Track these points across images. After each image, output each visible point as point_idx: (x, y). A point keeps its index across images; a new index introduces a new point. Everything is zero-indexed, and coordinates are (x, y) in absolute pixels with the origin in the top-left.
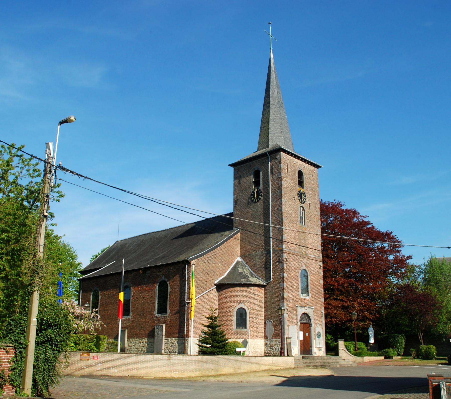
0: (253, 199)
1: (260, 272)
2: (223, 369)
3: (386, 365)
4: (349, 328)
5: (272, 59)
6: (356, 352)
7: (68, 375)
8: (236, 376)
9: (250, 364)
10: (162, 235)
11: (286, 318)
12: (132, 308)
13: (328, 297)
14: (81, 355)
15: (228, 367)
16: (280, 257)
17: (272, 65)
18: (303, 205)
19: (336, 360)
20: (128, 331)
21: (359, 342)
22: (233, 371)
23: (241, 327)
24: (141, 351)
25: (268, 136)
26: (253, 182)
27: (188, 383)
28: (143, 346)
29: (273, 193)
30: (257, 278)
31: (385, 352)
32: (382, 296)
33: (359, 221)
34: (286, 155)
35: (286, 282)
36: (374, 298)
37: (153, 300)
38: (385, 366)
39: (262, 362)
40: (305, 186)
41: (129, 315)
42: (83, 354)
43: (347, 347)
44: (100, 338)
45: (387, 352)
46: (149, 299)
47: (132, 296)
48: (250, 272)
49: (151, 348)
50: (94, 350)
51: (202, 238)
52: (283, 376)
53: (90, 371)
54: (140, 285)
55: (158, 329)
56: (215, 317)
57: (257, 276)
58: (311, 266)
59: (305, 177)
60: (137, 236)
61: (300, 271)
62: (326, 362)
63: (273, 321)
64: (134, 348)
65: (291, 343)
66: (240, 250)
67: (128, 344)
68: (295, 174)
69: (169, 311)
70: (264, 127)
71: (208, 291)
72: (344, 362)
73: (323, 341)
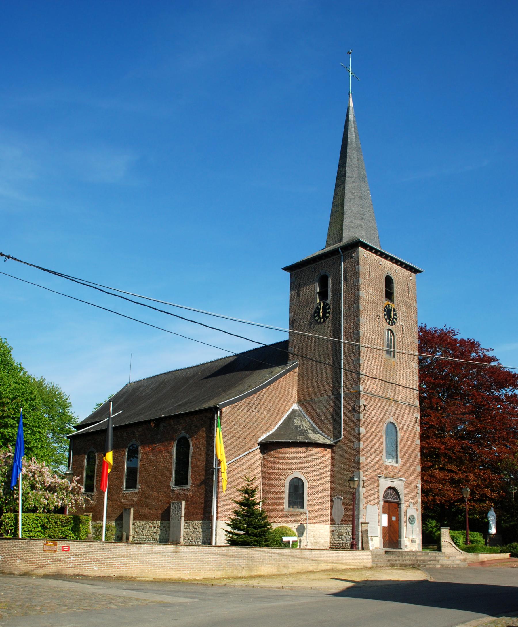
0: (317, 318)
1: (326, 426)
2: (260, 567)
3: (511, 567)
4: (461, 512)
5: (351, 109)
6: (467, 546)
7: (26, 574)
8: (278, 579)
9: (303, 560)
10: (190, 374)
11: (362, 494)
12: (140, 476)
13: (431, 465)
14: (45, 544)
15: (269, 565)
16: (355, 403)
17: (351, 117)
18: (392, 328)
19: (435, 557)
20: (134, 511)
21: (473, 531)
22: (275, 570)
23: (296, 506)
24: (152, 540)
25: (342, 225)
26: (318, 292)
27: (201, 588)
28: (155, 533)
29: (347, 309)
30: (321, 434)
31: (512, 547)
32: (510, 466)
33: (479, 356)
34: (368, 252)
35: (363, 441)
36: (498, 468)
37: (169, 466)
38: (510, 568)
39: (321, 558)
40: (395, 299)
41: (135, 487)
42: (47, 543)
43: (453, 538)
44: (80, 519)
45: (515, 548)
46: (163, 464)
47: (141, 460)
48: (312, 425)
49: (165, 534)
50: (70, 536)
51: (244, 376)
52: (351, 579)
53: (57, 569)
54: (152, 444)
55: (175, 508)
56: (252, 489)
57: (321, 432)
58: (401, 417)
59: (396, 287)
60: (156, 376)
61: (385, 425)
62: (420, 561)
63: (343, 498)
64: (143, 534)
65: (368, 530)
66: (297, 393)
67: (135, 529)
68: (380, 281)
69: (190, 482)
70: (336, 212)
71: (248, 452)
72: (448, 560)
73: (418, 529)
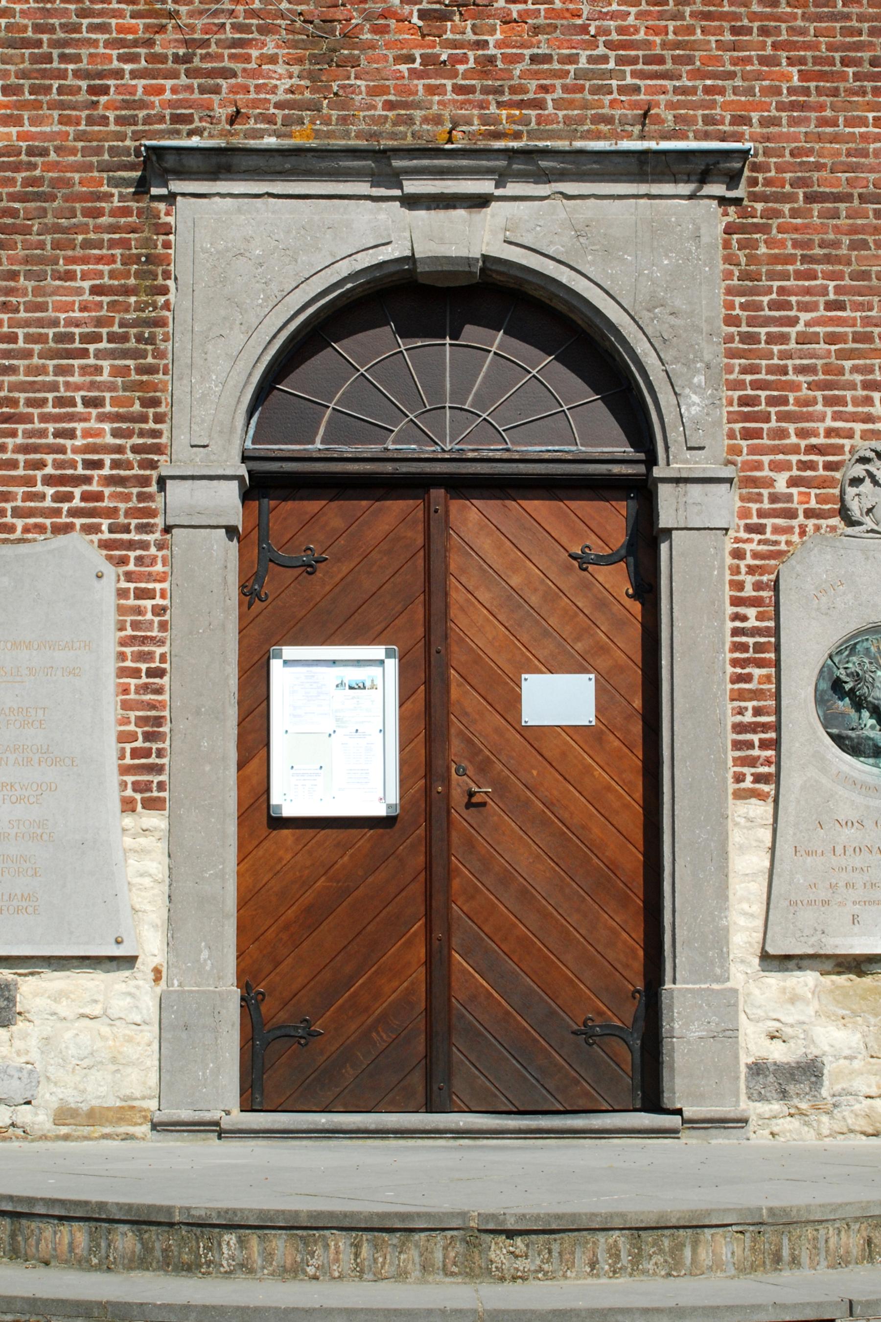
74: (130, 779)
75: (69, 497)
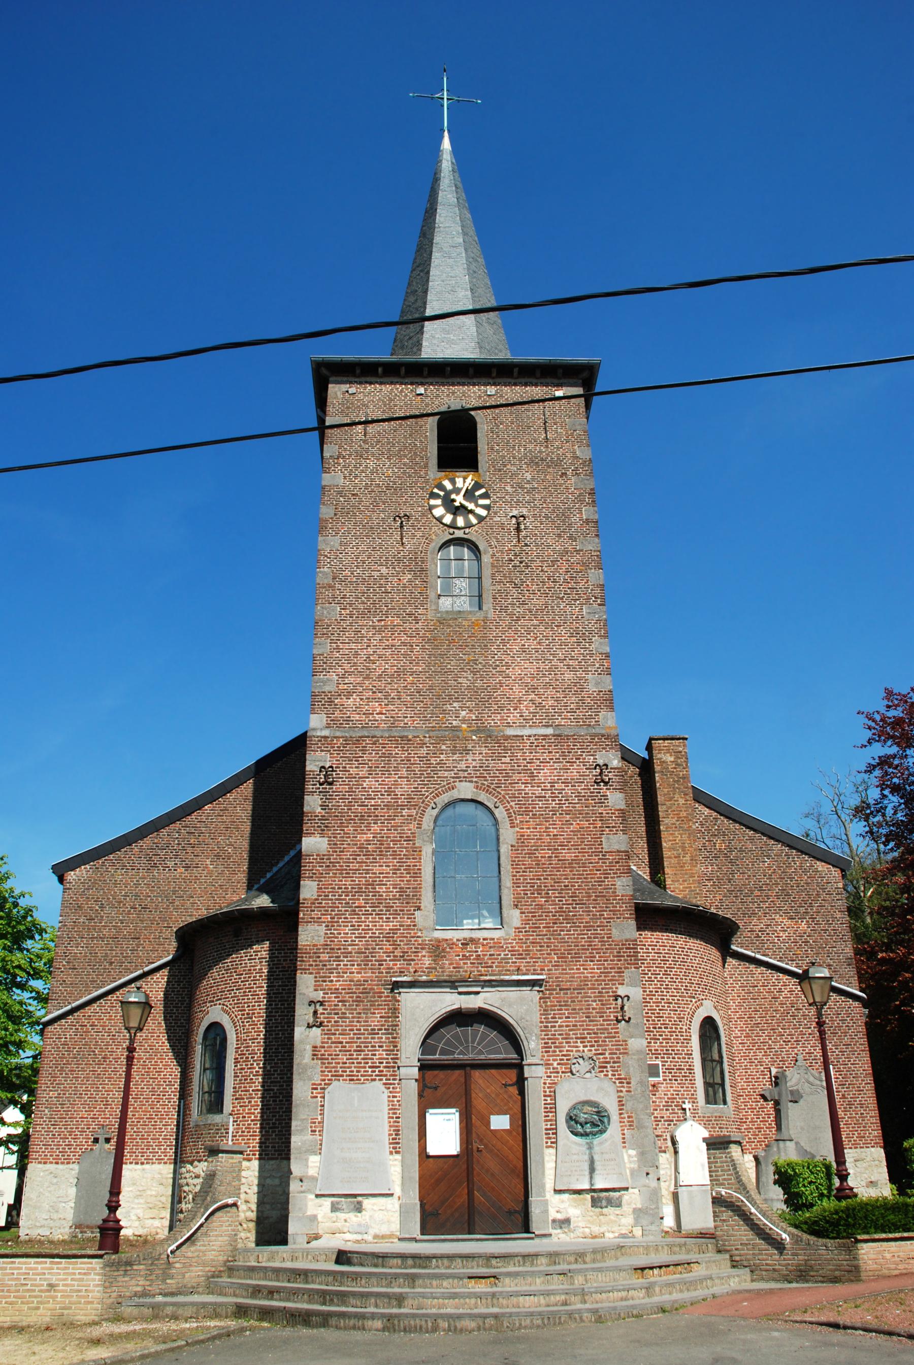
11: (309, 1048)
74: (392, 1146)
75: (375, 1071)
